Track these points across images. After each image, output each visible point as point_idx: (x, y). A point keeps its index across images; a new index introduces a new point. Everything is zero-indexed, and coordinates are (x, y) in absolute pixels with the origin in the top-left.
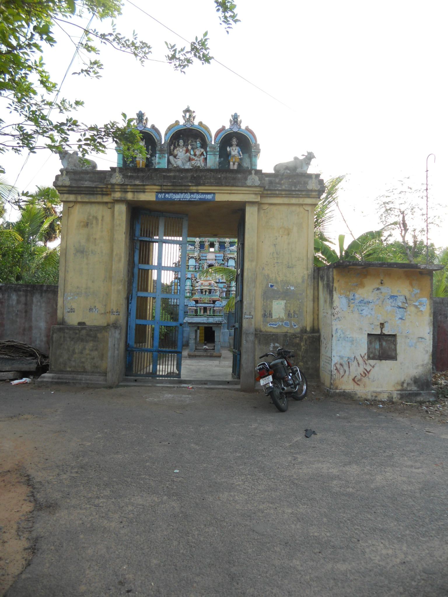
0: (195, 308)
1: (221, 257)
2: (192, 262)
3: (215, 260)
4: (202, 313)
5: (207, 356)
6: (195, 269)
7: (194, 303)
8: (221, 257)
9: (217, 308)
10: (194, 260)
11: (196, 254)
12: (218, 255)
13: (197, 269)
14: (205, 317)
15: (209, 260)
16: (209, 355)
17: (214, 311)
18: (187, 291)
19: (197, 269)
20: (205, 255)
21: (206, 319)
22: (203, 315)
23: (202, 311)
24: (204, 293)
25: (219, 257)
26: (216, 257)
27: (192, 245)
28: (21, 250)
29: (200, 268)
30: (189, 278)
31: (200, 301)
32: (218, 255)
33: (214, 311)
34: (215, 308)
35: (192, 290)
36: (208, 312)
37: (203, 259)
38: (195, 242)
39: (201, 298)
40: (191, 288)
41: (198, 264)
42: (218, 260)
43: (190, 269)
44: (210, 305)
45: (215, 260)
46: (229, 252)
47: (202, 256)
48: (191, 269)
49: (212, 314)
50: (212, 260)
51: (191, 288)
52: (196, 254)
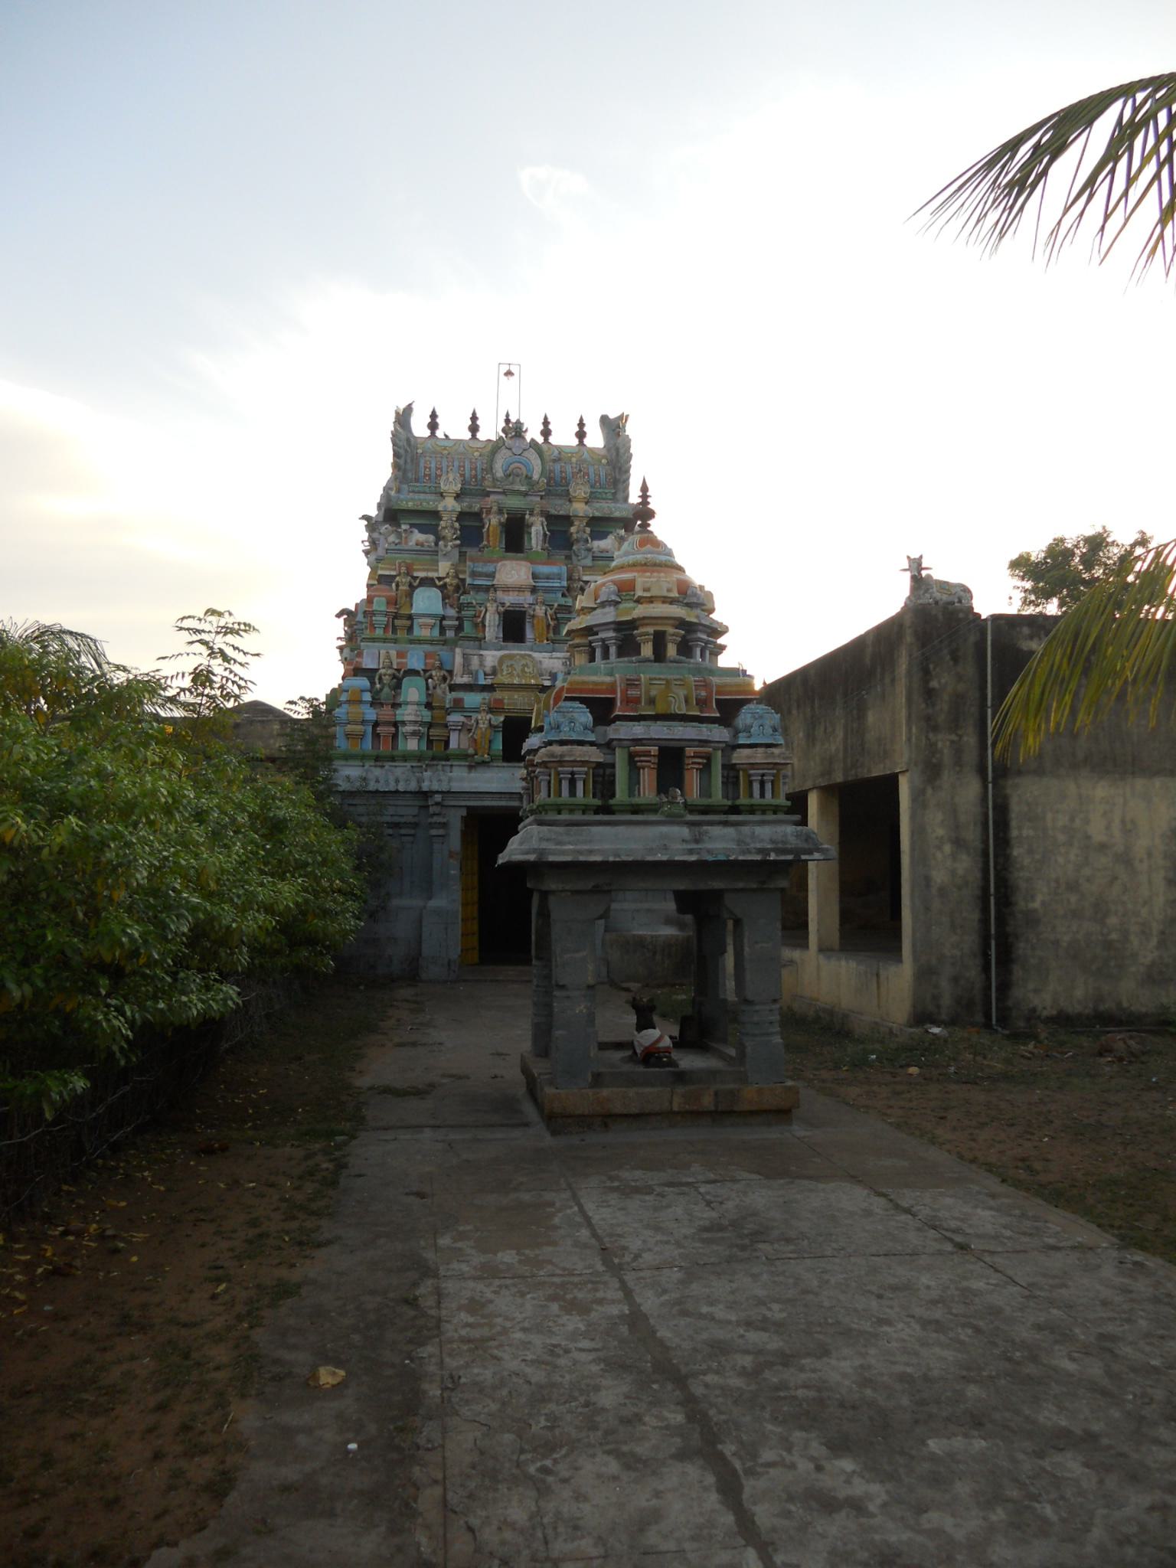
0: (595, 755)
1: (559, 577)
2: (427, 602)
3: (534, 590)
4: (648, 792)
5: (694, 1116)
6: (443, 630)
7: (585, 717)
8: (559, 577)
9: (759, 756)
10: (435, 594)
11: (444, 568)
12: (545, 569)
13: (450, 634)
14: (673, 820)
15: (507, 589)
16: (707, 1102)
17: (732, 773)
18: (409, 728)
19: (450, 634)
20: (489, 568)
21: (685, 832)
22: (653, 809)
23: (648, 778)
24: (647, 650)
25: (548, 577)
26: (535, 576)
27: (423, 529)
28: (28, 772)
29: (467, 625)
30: (414, 672)
31: (629, 701)
32: (545, 569)
33: (732, 773)
34: (740, 757)
35: (430, 725)
36: (693, 779)
37: (478, 588)
38: (436, 515)
39: (631, 684)
40: (427, 715)
41: (452, 612)
42: (547, 590)
43: (418, 632)
44: (706, 732)
45: (534, 590)
46: (588, 562)
47: (474, 574)
48: (425, 633)
49: (718, 796)
50: (520, 589)
51: (427, 715)
52: (444, 568)
